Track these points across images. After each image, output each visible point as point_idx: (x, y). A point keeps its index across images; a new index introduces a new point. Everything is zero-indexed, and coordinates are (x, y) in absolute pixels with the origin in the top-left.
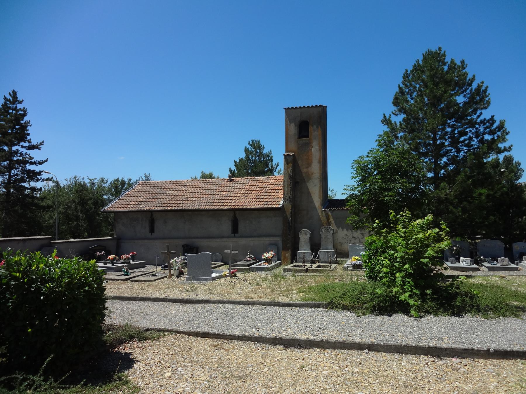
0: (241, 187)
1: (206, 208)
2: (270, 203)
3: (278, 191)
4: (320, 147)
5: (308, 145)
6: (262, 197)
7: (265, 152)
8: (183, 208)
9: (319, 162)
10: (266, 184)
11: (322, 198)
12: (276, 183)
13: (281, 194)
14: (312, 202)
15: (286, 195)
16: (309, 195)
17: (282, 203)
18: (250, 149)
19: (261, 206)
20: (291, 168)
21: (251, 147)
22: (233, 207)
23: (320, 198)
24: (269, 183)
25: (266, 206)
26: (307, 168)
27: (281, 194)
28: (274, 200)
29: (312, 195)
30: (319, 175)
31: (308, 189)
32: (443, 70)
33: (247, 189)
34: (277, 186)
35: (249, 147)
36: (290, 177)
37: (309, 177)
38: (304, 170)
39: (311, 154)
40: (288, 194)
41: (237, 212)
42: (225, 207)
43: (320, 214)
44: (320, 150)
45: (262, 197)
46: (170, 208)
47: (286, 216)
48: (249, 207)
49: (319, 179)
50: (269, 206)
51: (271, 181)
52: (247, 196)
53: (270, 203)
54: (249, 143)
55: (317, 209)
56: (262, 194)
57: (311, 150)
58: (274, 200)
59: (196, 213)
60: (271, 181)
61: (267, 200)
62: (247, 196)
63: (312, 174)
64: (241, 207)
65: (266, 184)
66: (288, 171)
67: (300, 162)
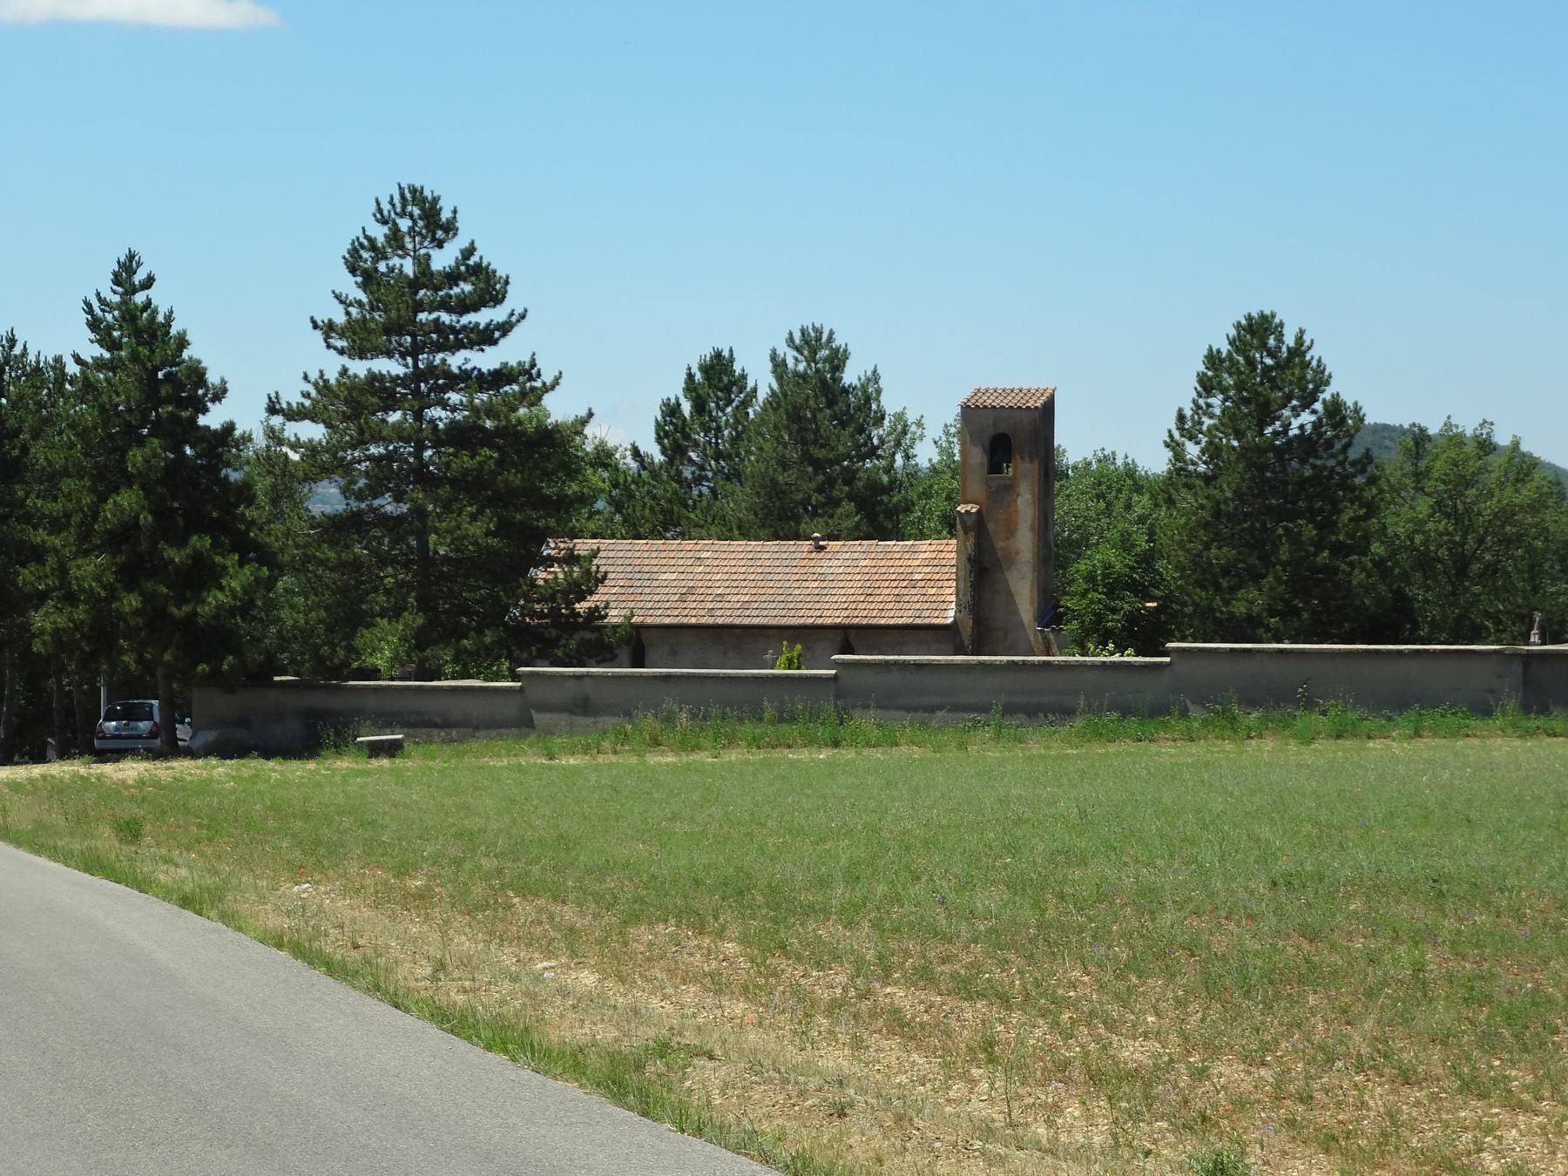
0: (849, 570)
1: (784, 621)
2: (927, 614)
3: (940, 584)
4: (1033, 496)
5: (1009, 488)
6: (907, 599)
7: (851, 376)
8: (729, 621)
9: (1032, 528)
10: (909, 563)
11: (1036, 605)
12: (936, 562)
13: (949, 593)
14: (1016, 612)
15: (961, 596)
16: (1010, 596)
17: (952, 613)
18: (790, 363)
19: (910, 621)
20: (972, 540)
21: (795, 354)
22: (847, 621)
23: (1032, 604)
24: (918, 563)
25: (918, 621)
26: (1008, 539)
27: (948, 591)
28: (934, 606)
29: (1016, 598)
30: (1031, 556)
31: (1007, 585)
32: (1133, 479)
33: (867, 577)
34: (937, 569)
35: (790, 356)
36: (969, 559)
37: (1010, 559)
38: (1000, 544)
39: (1016, 511)
40: (965, 594)
41: (852, 633)
42: (829, 621)
43: (1032, 638)
44: (1034, 503)
45: (907, 599)
46: (693, 621)
47: (962, 642)
48: (883, 622)
49: (1030, 565)
50: (927, 621)
51: (922, 556)
52: (871, 595)
53: (927, 614)
54: (791, 340)
55: (1026, 625)
56: (906, 592)
57: (1016, 501)
58: (934, 606)
59: (771, 632)
60: (922, 556)
61: (918, 606)
62: (871, 595)
63: (1017, 553)
64: (864, 622)
65: (909, 563)
66: (965, 545)
67: (991, 526)
